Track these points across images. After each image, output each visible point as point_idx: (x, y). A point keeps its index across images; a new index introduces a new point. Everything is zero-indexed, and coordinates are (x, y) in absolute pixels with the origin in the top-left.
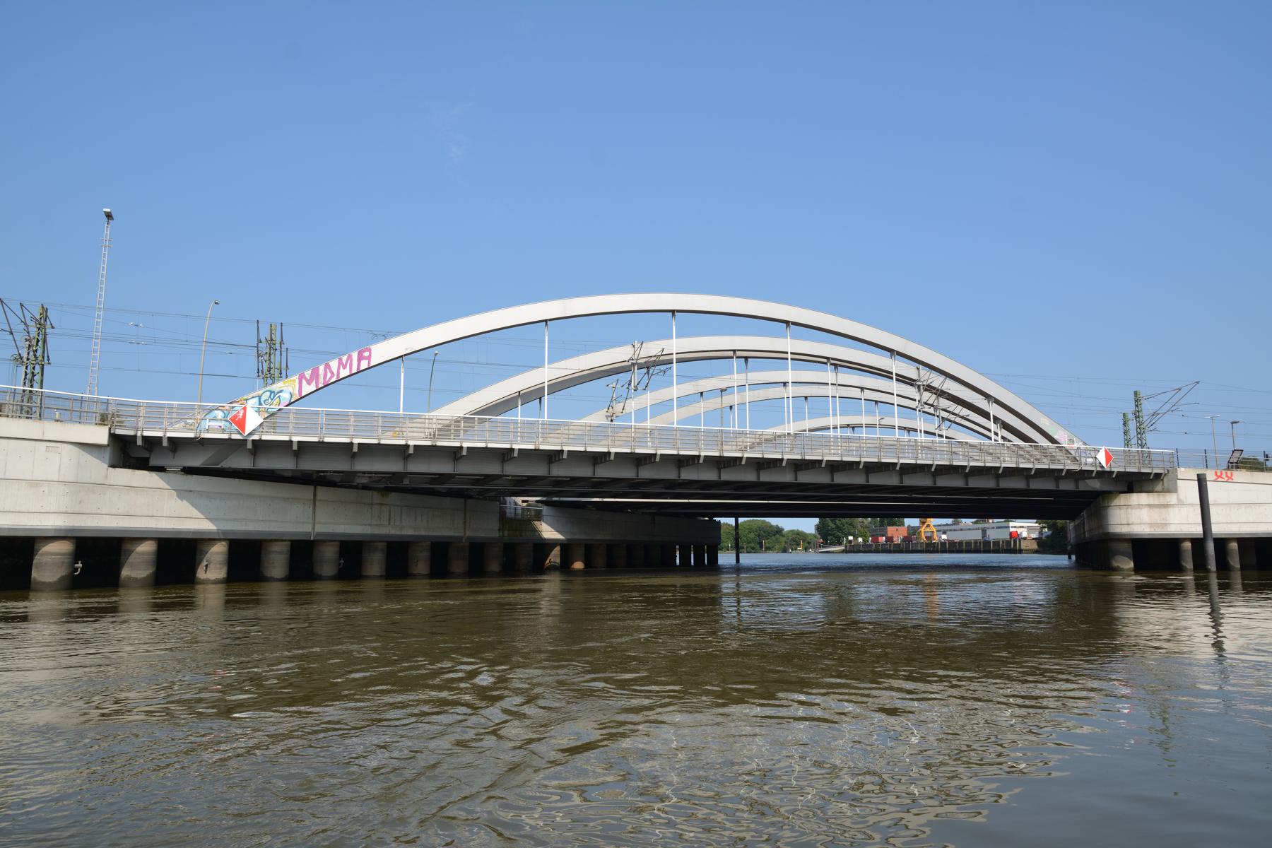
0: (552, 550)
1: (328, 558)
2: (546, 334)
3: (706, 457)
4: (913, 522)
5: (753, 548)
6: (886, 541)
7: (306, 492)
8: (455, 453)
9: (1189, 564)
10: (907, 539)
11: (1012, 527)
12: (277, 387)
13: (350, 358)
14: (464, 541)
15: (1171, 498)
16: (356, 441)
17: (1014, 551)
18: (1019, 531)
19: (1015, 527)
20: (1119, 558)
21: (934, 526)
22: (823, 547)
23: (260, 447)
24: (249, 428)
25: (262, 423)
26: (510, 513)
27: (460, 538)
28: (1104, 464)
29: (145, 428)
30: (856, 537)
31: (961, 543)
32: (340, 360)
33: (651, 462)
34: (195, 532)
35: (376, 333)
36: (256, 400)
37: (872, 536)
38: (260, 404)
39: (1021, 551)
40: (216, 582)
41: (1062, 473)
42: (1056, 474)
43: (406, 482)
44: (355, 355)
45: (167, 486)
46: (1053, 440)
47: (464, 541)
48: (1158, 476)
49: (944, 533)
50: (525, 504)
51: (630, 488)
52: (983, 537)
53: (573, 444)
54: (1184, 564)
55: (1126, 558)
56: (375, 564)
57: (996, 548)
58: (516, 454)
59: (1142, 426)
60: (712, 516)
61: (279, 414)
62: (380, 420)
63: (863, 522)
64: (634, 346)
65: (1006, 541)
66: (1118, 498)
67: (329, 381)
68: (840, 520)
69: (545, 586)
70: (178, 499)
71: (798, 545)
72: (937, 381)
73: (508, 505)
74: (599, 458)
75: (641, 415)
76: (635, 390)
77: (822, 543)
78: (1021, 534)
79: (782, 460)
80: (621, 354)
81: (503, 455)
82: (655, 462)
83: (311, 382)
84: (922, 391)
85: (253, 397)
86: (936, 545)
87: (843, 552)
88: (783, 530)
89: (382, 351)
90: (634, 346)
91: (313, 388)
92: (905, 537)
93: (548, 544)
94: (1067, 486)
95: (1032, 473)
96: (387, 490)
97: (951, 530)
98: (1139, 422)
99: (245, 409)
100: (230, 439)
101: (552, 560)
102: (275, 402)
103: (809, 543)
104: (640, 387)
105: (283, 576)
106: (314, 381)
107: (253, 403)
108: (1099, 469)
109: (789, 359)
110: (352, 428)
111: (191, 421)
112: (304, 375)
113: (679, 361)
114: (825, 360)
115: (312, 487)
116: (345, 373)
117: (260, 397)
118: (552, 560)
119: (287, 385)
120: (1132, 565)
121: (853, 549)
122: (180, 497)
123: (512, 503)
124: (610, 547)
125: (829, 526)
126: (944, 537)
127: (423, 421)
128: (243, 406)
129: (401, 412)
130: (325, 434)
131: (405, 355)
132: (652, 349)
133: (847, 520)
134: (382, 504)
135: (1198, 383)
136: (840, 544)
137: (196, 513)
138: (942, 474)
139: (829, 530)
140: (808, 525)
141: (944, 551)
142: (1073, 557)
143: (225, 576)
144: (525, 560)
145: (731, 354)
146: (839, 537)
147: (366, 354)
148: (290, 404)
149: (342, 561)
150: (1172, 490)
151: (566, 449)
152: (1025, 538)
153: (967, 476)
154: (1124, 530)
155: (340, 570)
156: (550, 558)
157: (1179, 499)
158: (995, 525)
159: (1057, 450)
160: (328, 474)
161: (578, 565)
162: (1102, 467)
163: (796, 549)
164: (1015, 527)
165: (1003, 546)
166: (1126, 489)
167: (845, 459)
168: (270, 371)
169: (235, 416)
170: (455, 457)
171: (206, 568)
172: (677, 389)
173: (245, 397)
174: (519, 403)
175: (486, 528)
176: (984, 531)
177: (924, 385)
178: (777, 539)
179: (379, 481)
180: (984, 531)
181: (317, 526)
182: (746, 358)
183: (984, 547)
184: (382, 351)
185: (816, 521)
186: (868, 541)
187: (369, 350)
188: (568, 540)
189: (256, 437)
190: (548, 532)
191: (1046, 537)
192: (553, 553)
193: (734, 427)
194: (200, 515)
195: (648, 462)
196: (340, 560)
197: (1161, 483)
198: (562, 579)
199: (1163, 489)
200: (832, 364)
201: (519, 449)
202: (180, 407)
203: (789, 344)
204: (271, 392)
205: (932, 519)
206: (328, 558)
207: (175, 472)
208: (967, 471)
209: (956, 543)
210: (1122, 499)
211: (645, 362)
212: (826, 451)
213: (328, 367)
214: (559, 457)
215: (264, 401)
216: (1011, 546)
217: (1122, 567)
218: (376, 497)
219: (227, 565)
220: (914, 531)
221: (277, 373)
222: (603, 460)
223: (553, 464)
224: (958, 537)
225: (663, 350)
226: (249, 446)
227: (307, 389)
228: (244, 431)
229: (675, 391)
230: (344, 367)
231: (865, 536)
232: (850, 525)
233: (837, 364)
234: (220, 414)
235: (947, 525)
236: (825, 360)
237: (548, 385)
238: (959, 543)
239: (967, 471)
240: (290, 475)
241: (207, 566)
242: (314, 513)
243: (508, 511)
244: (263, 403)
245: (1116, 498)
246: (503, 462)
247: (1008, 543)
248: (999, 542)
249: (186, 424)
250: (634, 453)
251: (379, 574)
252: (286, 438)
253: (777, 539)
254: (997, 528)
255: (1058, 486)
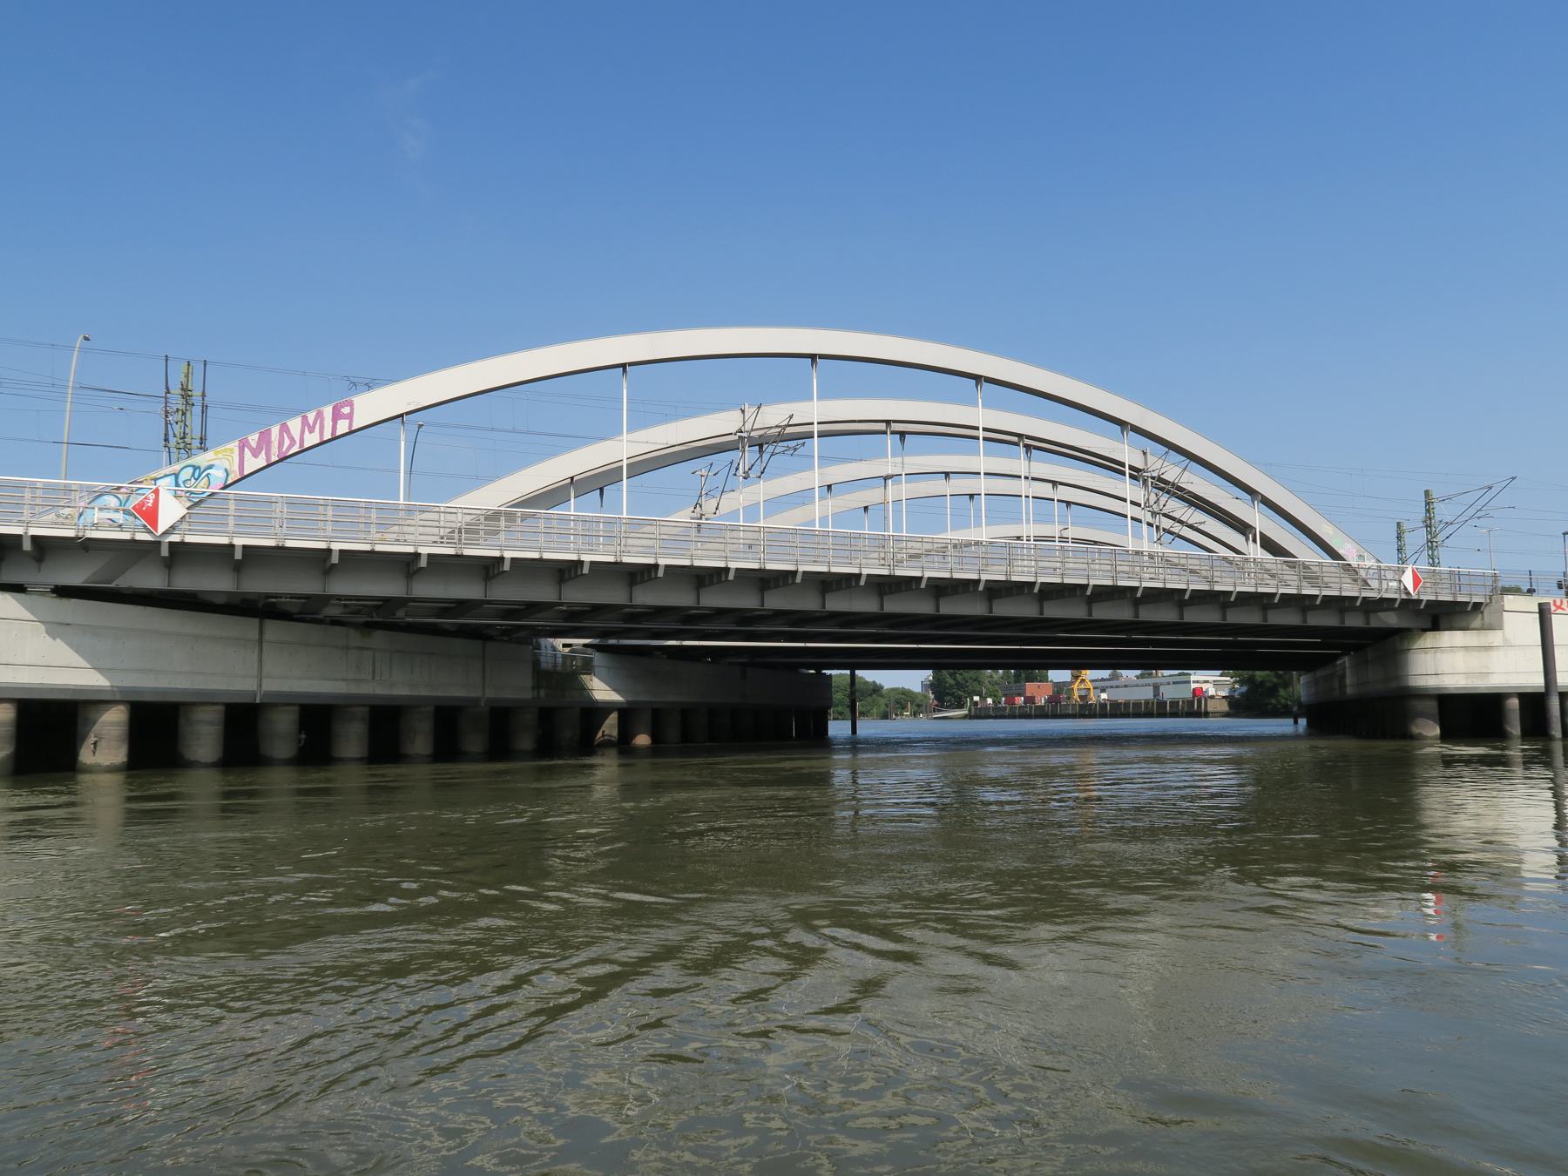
0: (606, 718)
1: (281, 734)
2: (625, 385)
3: (805, 573)
4: (1059, 676)
5: (841, 714)
6: (1025, 702)
7: (247, 627)
8: (408, 565)
9: (1515, 728)
10: (1054, 700)
11: (1194, 682)
12: (202, 459)
13: (320, 415)
14: (482, 704)
15: (1494, 637)
16: (336, 546)
17: (1198, 714)
18: (1205, 687)
19: (1198, 682)
20: (1420, 721)
21: (1092, 681)
22: (939, 711)
23: (182, 553)
24: (163, 526)
25: (184, 516)
26: (546, 663)
27: (476, 701)
28: (1411, 589)
29: (983, 570)
30: (983, 698)
31: (1127, 704)
32: (305, 418)
33: (650, 579)
34: (77, 690)
35: (355, 380)
36: (171, 479)
37: (1005, 695)
38: (177, 485)
39: (1206, 714)
40: (112, 769)
41: (1316, 600)
42: (1222, 600)
43: (400, 613)
44: (328, 411)
45: (28, 616)
46: (1334, 554)
47: (482, 704)
48: (1477, 607)
49: (1103, 690)
50: (567, 650)
51: (738, 625)
52: (1154, 696)
53: (675, 556)
54: (1509, 729)
55: (1432, 722)
56: (351, 740)
57: (1174, 710)
58: (586, 570)
59: (1434, 540)
60: (819, 667)
61: (210, 503)
62: (330, 512)
63: (991, 676)
64: (743, 411)
65: (1188, 701)
66: (1422, 639)
67: (286, 452)
68: (961, 674)
69: (600, 774)
70: (47, 637)
71: (904, 708)
72: (1172, 471)
73: (543, 651)
74: (639, 575)
75: (751, 511)
76: (745, 478)
77: (936, 706)
78: (1207, 691)
79: (794, 573)
80: (723, 423)
81: (486, 568)
82: (727, 580)
83: (260, 453)
84: (1150, 488)
85: (166, 476)
86: (1093, 707)
87: (965, 717)
88: (882, 687)
89: (371, 406)
90: (743, 411)
91: (261, 462)
92: (1050, 697)
93: (601, 709)
94: (1354, 621)
95: (1187, 597)
96: (370, 626)
97: (1112, 687)
98: (1430, 533)
99: (156, 492)
100: (133, 541)
101: (606, 733)
102: (202, 484)
103: (918, 706)
104: (752, 474)
105: (215, 760)
106: (263, 452)
107: (165, 485)
108: (1404, 597)
109: (981, 439)
110: (231, 521)
111: (67, 511)
112: (248, 441)
113: (822, 435)
114: (1015, 439)
115: (256, 621)
116: (311, 439)
117: (177, 476)
118: (606, 733)
119: (220, 456)
120: (1437, 731)
121: (979, 714)
122: (53, 635)
123: (549, 648)
124: (686, 712)
125: (946, 683)
126: (1104, 696)
127: (435, 516)
128: (154, 487)
129: (401, 502)
130: (465, 544)
131: (408, 413)
132: (773, 416)
133: (972, 673)
134: (361, 648)
135: (1514, 478)
136: (960, 706)
137: (78, 660)
138: (1052, 599)
139: (946, 688)
140: (914, 680)
141: (1103, 716)
142: (1303, 722)
143: (125, 759)
144: (568, 732)
145: (882, 427)
146: (960, 697)
147: (346, 410)
148: (225, 487)
149: (303, 736)
150: (1496, 626)
151: (662, 562)
152: (1212, 697)
153: (238, 567)
154: (1431, 682)
155: (301, 750)
156: (603, 728)
157: (1505, 639)
158: (1171, 680)
159: (1285, 567)
160: (283, 600)
161: (643, 740)
162: (1408, 593)
163: (902, 714)
164: (1198, 682)
165: (1183, 707)
166: (1429, 625)
167: (956, 576)
168: (184, 438)
169: (142, 504)
170: (409, 570)
171: (95, 748)
172: (820, 474)
173: (154, 475)
174: (572, 495)
175: (514, 686)
176: (1156, 688)
177: (1153, 478)
178: (873, 701)
179: (357, 613)
180: (1156, 688)
181: (264, 681)
182: (902, 434)
183: (1158, 709)
184: (371, 406)
185: (927, 675)
186: (1000, 703)
187: (351, 404)
188: (628, 702)
189: (175, 538)
190: (601, 690)
191: (1240, 694)
192: (607, 722)
193: (898, 527)
194: (84, 663)
195: (573, 575)
196: (300, 733)
197: (1480, 616)
198: (620, 761)
199: (1483, 624)
200: (893, 433)
201: (429, 555)
202: (47, 488)
203: (981, 416)
204: (195, 468)
205: (1088, 671)
206: (281, 734)
207: (43, 593)
208: (1139, 595)
209: (1121, 703)
210: (1429, 639)
211: (760, 436)
212: (1238, 581)
213: (285, 429)
214: (576, 572)
215: (184, 482)
216: (1194, 707)
217: (1425, 734)
218: (355, 638)
219: (127, 741)
220: (1059, 687)
221: (196, 443)
222: (646, 578)
223: (637, 587)
224: (1122, 696)
225: (791, 417)
226: (165, 552)
227: (252, 464)
228: (156, 528)
229: (815, 478)
230: (311, 431)
231: (995, 696)
232: (975, 680)
233: (1032, 445)
234: (111, 501)
235: (1103, 680)
236: (1015, 439)
237: (627, 465)
238: (1125, 704)
239: (1139, 595)
240: (220, 600)
241: (95, 744)
242: (260, 661)
243: (543, 659)
244: (182, 485)
245: (1420, 638)
246: (407, 577)
247: (1191, 703)
248: (1178, 702)
249: (58, 516)
250: (621, 563)
251: (359, 756)
252: (224, 541)
253: (873, 701)
254: (1174, 683)
255: (1265, 619)
